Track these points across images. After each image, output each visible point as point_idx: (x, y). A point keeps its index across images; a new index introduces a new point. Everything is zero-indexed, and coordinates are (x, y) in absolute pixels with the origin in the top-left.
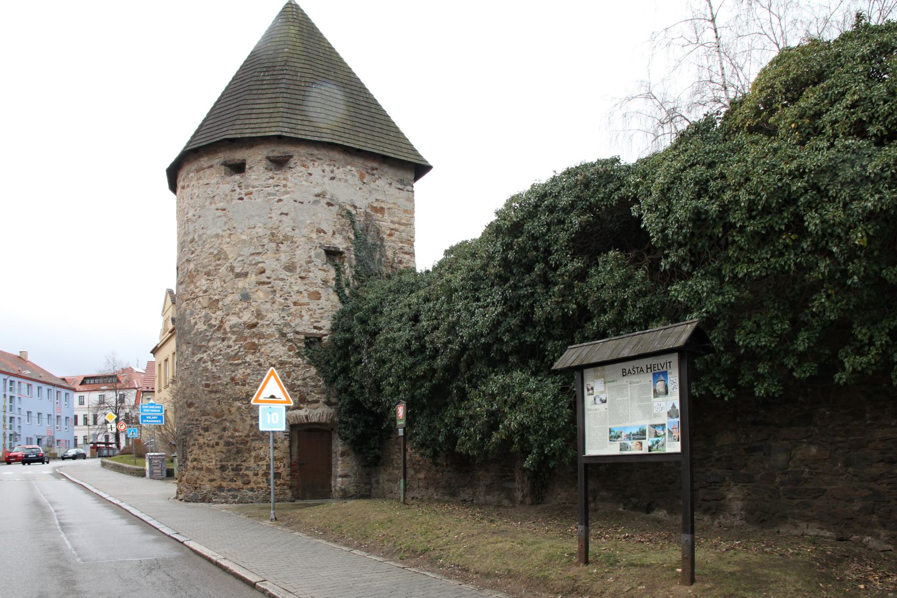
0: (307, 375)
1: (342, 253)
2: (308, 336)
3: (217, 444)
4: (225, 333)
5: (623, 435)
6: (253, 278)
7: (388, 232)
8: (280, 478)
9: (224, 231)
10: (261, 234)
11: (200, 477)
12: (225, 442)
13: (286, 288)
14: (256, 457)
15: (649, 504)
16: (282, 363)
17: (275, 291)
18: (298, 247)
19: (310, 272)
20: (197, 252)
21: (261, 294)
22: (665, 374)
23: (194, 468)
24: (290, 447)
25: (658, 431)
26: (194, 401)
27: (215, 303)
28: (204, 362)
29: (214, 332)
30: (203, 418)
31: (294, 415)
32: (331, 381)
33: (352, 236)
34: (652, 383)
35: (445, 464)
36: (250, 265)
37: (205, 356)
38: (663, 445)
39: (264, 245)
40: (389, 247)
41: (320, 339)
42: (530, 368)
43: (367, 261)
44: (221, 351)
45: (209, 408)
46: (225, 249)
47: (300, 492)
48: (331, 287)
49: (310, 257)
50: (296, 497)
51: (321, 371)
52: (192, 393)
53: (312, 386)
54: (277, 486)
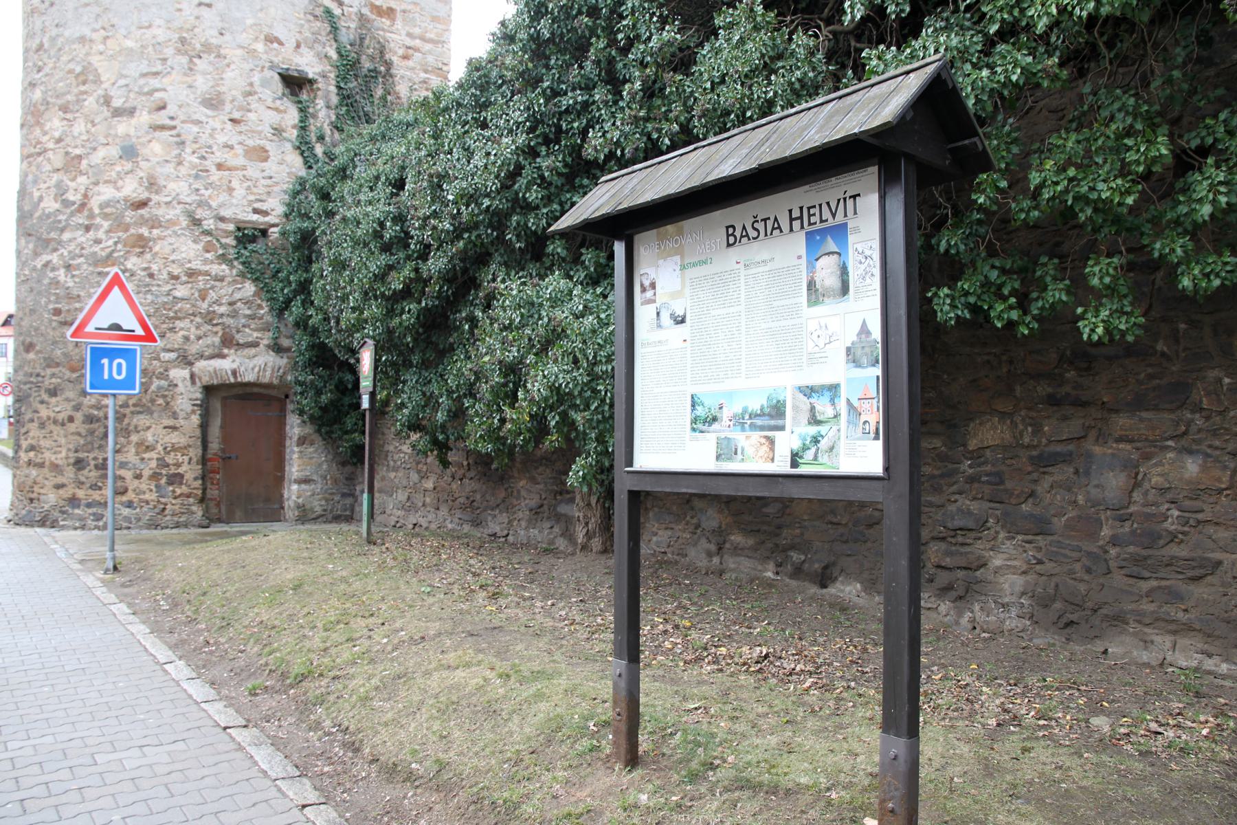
0: (237, 296)
1: (311, 82)
2: (242, 225)
3: (71, 419)
4: (91, 216)
5: (726, 414)
6: (144, 118)
7: (401, 52)
8: (181, 483)
9: (95, 30)
10: (161, 39)
11: (40, 479)
12: (85, 416)
13: (204, 139)
14: (139, 444)
15: (826, 568)
16: (192, 274)
17: (183, 143)
18: (228, 66)
19: (249, 111)
20: (47, 70)
21: (157, 147)
22: (840, 232)
23: (29, 463)
24: (204, 426)
25: (818, 407)
26: (35, 340)
27: (76, 161)
28: (53, 269)
29: (72, 214)
30: (49, 371)
31: (211, 369)
32: (281, 310)
33: (334, 56)
34: (804, 261)
35: (465, 463)
36: (140, 93)
37: (54, 258)
38: (832, 449)
39: (165, 60)
40: (402, 77)
41: (264, 233)
42: (586, 268)
43: (358, 97)
44: (83, 248)
45: (59, 352)
46: (96, 65)
47: (223, 508)
48: (290, 141)
49: (251, 84)
50: (210, 519)
51: (265, 289)
52: (31, 326)
53: (246, 316)
54: (175, 498)
